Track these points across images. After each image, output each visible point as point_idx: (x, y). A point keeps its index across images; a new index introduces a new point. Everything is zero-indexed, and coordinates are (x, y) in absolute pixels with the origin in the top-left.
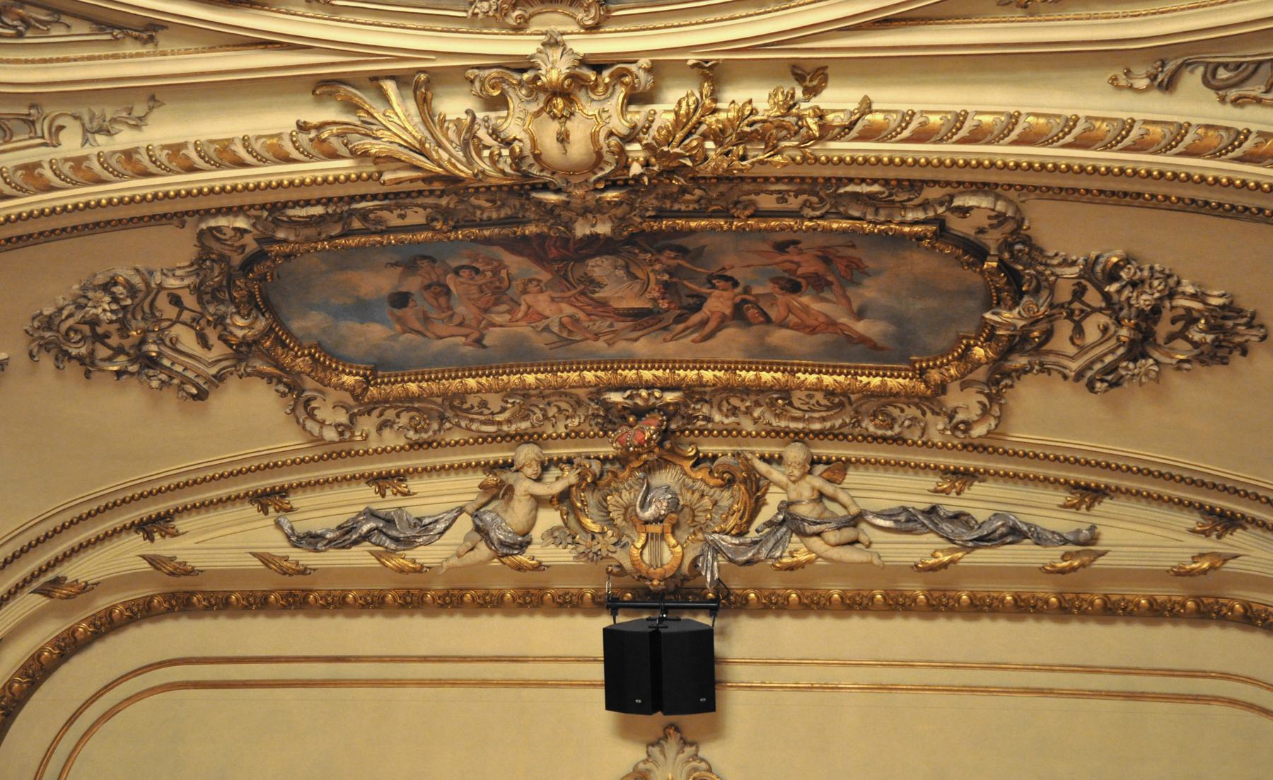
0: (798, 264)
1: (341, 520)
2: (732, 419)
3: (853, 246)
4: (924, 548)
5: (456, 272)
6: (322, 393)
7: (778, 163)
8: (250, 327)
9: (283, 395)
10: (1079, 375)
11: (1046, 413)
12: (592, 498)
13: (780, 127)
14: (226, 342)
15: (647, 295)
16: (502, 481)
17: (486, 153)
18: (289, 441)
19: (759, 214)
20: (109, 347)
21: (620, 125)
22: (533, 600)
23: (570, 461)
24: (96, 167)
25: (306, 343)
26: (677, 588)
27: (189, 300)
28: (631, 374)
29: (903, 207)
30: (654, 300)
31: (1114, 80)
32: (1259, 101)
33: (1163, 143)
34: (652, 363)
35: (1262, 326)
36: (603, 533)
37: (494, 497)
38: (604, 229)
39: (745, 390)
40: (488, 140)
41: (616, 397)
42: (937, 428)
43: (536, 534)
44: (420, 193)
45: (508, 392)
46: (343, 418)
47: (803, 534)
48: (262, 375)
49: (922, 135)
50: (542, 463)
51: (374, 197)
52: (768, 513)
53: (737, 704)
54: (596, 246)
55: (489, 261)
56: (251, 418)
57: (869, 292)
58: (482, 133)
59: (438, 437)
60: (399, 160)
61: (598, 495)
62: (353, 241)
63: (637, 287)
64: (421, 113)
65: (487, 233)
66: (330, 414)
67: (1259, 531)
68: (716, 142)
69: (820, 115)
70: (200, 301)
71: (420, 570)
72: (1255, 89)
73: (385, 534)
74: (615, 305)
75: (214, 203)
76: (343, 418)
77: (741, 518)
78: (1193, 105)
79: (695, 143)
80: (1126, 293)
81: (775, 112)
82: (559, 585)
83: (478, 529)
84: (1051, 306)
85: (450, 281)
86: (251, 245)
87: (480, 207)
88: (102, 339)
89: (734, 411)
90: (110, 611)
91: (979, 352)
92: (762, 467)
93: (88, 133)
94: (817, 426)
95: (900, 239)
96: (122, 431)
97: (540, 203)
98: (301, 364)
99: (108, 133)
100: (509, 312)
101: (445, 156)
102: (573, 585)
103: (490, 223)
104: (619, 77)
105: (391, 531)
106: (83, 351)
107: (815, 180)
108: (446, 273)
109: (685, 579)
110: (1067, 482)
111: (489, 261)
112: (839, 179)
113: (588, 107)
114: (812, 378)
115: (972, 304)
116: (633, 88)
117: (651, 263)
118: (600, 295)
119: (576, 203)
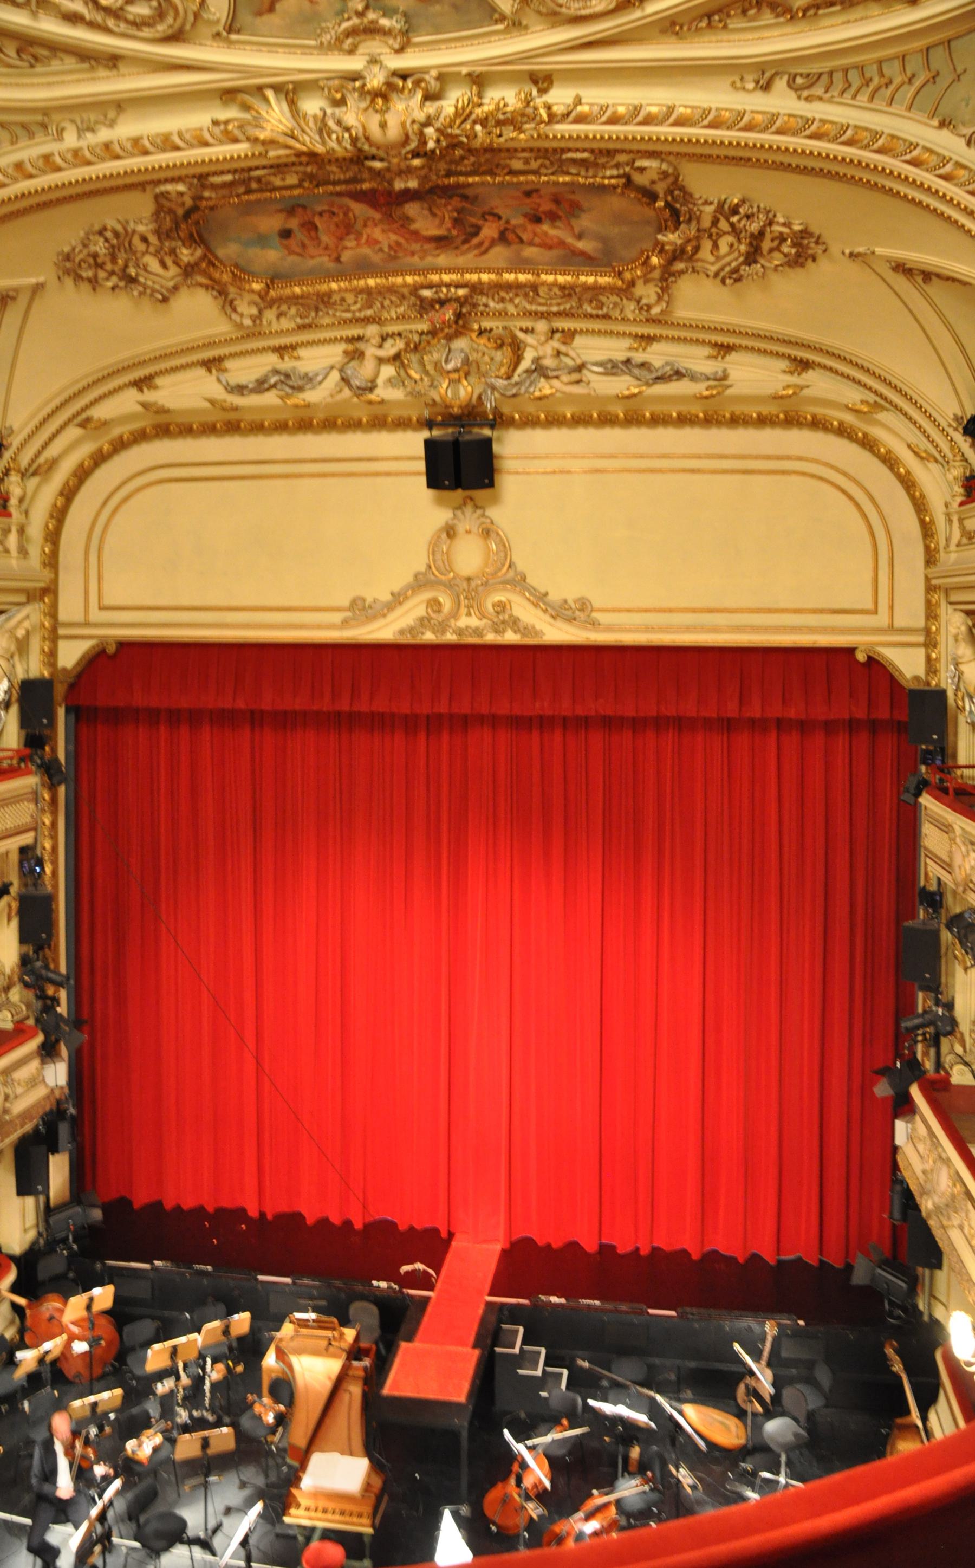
0: (539, 205)
3: (574, 192)
4: (623, 384)
5: (321, 214)
6: (241, 295)
9: (216, 298)
10: (716, 275)
11: (697, 298)
12: (414, 358)
13: (523, 115)
16: (357, 349)
17: (334, 136)
18: (221, 327)
19: (512, 172)
20: (106, 271)
21: (421, 116)
22: (379, 423)
23: (400, 335)
24: (87, 154)
25: (227, 263)
26: (470, 414)
27: (153, 239)
28: (435, 278)
29: (604, 167)
31: (733, 84)
32: (820, 99)
33: (763, 125)
34: (449, 270)
35: (824, 243)
36: (422, 379)
37: (353, 359)
38: (413, 184)
39: (509, 287)
41: (427, 293)
42: (630, 308)
43: (380, 381)
45: (358, 292)
46: (254, 311)
47: (547, 377)
48: (201, 285)
49: (614, 120)
51: (264, 167)
54: (408, 196)
55: (340, 207)
57: (584, 222)
58: (331, 124)
60: (278, 142)
61: (418, 356)
62: (252, 197)
63: (437, 221)
64: (291, 110)
66: (246, 309)
67: (822, 371)
68: (482, 125)
69: (548, 107)
70: (159, 238)
71: (308, 406)
72: (818, 90)
73: (287, 384)
75: (162, 175)
76: (254, 311)
78: (781, 101)
80: (743, 222)
81: (520, 105)
82: (394, 413)
83: (343, 379)
84: (699, 230)
85: (317, 220)
86: (189, 202)
87: (333, 172)
88: (101, 266)
89: (502, 300)
90: (121, 437)
91: (655, 260)
92: (521, 335)
93: (80, 133)
94: (555, 309)
95: (603, 188)
96: (115, 325)
97: (371, 169)
98: (226, 277)
102: (405, 413)
103: (339, 182)
104: (417, 83)
105: (290, 382)
107: (546, 150)
108: (314, 215)
109: (474, 407)
110: (710, 342)
111: (340, 207)
114: (550, 278)
115: (650, 229)
116: (427, 90)
117: (445, 206)
118: (414, 227)
119: (394, 168)
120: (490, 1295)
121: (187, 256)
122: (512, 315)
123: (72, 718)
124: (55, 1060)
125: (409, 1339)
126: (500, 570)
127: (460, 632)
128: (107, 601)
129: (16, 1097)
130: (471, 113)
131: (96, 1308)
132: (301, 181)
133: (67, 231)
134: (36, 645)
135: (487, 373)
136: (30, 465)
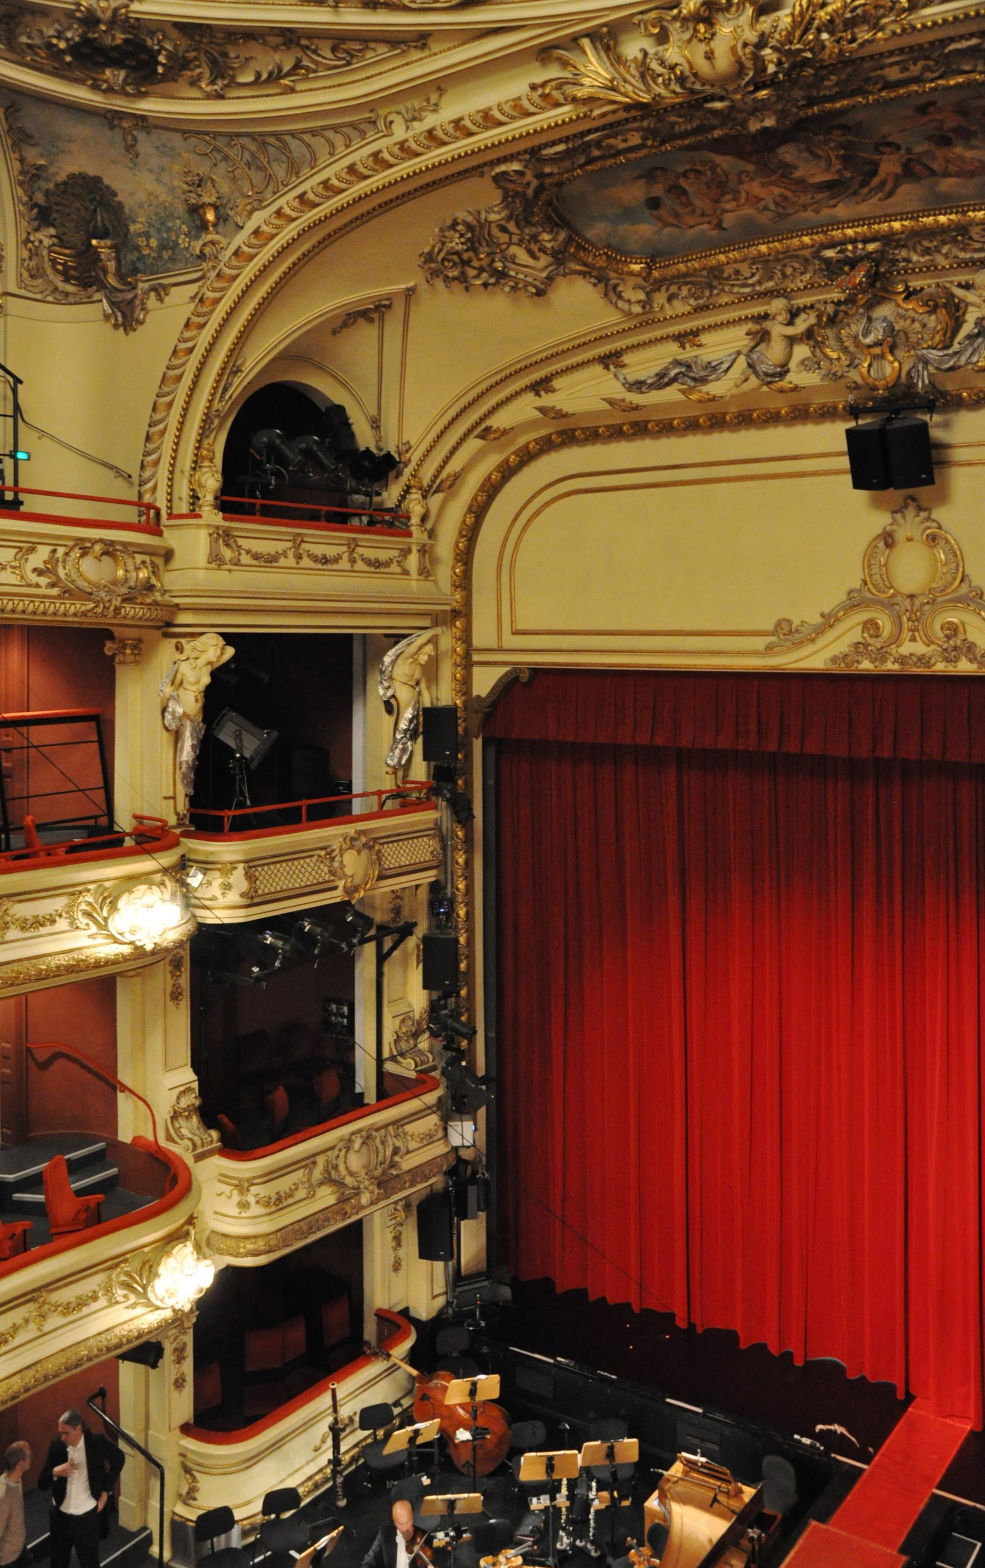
1: (657, 369)
2: (927, 258)
5: (685, 174)
7: (881, 39)
8: (553, 240)
9: (595, 285)
12: (830, 333)
14: (545, 252)
15: (833, 169)
17: (660, 80)
18: (610, 318)
19: (888, 85)
21: (751, 36)
23: (812, 307)
27: (511, 226)
28: (837, 234)
30: (839, 172)
36: (839, 359)
38: (769, 122)
40: (659, 70)
41: (830, 253)
43: (793, 365)
44: (627, 120)
46: (642, 296)
50: (790, 312)
51: (596, 130)
52: (968, 328)
53: (961, 481)
56: (579, 306)
58: (654, 65)
59: (711, 301)
60: (599, 99)
63: (823, 164)
65: (687, 142)
71: (713, 399)
74: (812, 181)
76: (642, 296)
77: (945, 335)
79: (811, 37)
82: (818, 401)
83: (750, 366)
85: (683, 183)
88: (467, 263)
89: (927, 251)
90: (527, 446)
92: (959, 292)
97: (715, 112)
99: (421, 120)
100: (734, 199)
101: (630, 88)
102: (830, 400)
103: (682, 136)
105: (688, 374)
106: (456, 273)
107: (921, 46)
111: (704, 163)
112: (941, 41)
113: (725, 29)
117: (826, 142)
118: (798, 174)
120: (939, 1488)
121: (550, 241)
122: (944, 267)
123: (492, 752)
124: (464, 1117)
125: (823, 1520)
126: (951, 584)
127: (902, 660)
128: (520, 626)
129: (408, 1152)
130: (813, 19)
131: (480, 1397)
132: (644, 138)
133: (421, 230)
134: (447, 671)
135: (918, 344)
136: (433, 481)
